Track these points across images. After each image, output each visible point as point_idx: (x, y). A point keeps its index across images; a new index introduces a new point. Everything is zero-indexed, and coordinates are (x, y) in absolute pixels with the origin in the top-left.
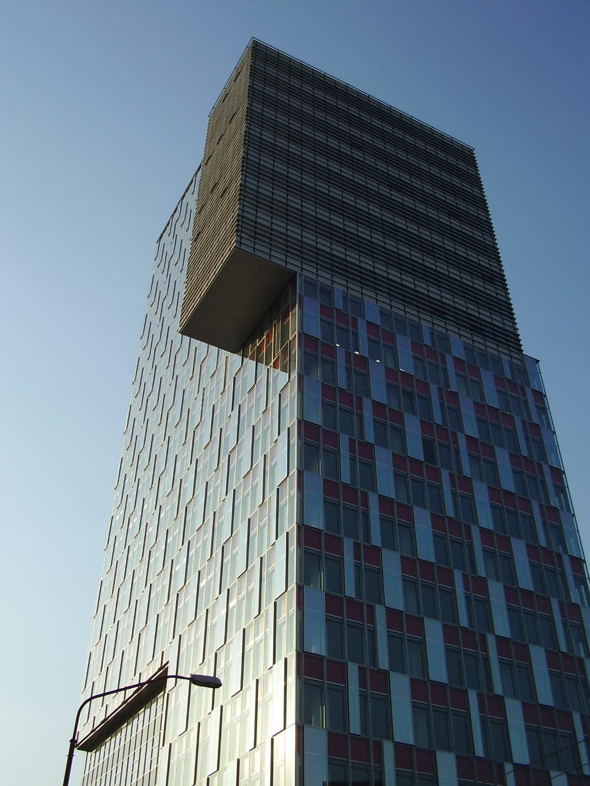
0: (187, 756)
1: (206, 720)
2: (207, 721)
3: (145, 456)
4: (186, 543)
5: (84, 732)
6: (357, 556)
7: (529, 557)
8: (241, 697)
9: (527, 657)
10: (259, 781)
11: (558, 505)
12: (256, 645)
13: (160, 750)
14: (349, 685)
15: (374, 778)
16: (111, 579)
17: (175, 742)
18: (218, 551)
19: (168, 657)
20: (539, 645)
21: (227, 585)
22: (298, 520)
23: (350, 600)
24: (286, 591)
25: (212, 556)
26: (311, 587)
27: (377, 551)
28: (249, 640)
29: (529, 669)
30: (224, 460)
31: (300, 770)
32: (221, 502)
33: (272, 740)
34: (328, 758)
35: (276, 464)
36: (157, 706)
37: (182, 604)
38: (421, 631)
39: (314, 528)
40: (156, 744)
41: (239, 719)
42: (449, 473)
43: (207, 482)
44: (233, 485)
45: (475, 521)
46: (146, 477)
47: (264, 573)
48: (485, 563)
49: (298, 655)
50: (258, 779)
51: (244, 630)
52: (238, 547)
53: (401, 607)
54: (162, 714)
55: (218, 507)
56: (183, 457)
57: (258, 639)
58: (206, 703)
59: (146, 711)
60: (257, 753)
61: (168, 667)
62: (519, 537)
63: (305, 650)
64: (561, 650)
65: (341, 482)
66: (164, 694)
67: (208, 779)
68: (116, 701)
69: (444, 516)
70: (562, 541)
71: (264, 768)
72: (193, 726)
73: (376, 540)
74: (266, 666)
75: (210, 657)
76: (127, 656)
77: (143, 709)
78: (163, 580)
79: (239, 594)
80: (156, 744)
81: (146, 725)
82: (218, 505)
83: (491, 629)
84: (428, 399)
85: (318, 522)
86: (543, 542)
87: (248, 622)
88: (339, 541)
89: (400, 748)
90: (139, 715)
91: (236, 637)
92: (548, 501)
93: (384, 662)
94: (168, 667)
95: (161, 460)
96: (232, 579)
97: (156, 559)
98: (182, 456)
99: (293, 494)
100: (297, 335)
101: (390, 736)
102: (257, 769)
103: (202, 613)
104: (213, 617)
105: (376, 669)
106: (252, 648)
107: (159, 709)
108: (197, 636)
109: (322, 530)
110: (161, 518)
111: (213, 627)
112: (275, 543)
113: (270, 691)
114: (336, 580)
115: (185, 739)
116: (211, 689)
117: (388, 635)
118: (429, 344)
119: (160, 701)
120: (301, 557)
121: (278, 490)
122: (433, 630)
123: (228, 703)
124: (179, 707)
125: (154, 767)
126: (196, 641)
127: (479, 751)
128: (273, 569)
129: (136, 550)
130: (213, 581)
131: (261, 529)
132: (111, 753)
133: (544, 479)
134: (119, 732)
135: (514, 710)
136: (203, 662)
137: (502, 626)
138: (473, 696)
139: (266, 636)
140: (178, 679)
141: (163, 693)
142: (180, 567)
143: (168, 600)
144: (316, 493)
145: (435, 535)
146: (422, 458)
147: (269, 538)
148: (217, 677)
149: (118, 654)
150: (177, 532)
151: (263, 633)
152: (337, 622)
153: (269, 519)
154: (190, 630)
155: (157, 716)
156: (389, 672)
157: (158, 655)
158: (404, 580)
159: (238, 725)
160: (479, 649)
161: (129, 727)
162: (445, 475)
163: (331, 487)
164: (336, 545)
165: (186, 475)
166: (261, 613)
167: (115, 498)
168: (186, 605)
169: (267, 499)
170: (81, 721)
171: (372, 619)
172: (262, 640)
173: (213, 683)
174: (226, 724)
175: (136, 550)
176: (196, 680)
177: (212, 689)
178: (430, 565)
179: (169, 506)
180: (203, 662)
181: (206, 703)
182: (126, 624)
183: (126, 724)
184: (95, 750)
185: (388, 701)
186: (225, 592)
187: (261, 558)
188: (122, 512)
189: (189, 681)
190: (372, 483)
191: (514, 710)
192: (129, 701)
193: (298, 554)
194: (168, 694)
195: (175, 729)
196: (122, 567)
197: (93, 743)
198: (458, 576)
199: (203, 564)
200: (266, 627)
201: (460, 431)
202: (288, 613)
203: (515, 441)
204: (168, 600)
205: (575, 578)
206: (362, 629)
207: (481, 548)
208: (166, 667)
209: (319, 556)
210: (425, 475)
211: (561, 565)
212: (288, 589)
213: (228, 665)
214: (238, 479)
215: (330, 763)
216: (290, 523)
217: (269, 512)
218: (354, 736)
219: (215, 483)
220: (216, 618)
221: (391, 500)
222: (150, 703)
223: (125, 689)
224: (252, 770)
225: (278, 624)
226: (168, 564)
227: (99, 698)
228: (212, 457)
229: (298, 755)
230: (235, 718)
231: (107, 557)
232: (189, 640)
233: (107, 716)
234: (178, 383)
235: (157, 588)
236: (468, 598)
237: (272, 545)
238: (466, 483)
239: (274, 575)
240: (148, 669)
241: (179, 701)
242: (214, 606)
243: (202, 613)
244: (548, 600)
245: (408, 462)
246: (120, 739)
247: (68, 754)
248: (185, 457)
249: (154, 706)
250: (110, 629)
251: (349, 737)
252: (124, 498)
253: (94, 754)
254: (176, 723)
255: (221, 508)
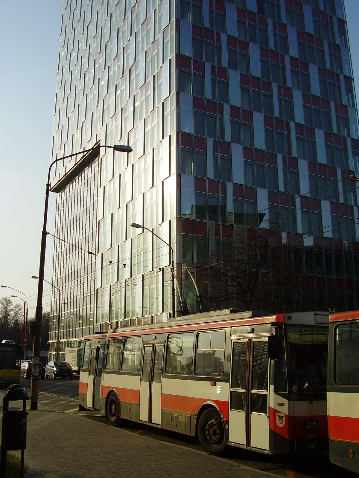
0: (114, 192)
1: (124, 172)
2: (125, 172)
3: (77, 12)
4: (107, 68)
5: (54, 182)
6: (213, 73)
7: (320, 75)
8: (144, 159)
9: (313, 136)
10: (156, 205)
11: (340, 43)
12: (152, 128)
13: (99, 190)
14: (207, 150)
15: (221, 203)
16: (59, 137)
17: (107, 185)
18: (127, 72)
19: (100, 136)
20: (314, 64)
21: (133, 93)
22: (177, 50)
23: (206, 29)
24: (169, 96)
25: (124, 75)
26: (185, 93)
27: (225, 70)
28: (147, 123)
29: (314, 142)
30: (129, 14)
31: (179, 208)
32: (128, 41)
33: (163, 182)
34: (195, 192)
35: (162, 15)
36: (95, 165)
37: (107, 105)
38: (251, 119)
39: (186, 56)
40: (96, 187)
41: (143, 171)
42: (273, 21)
43: (118, 28)
44: (135, 30)
45: (287, 52)
46: (79, 27)
47: (156, 85)
48: (292, 77)
49: (177, 133)
50: (155, 204)
51: (145, 119)
52: (139, 69)
53: (239, 105)
54: (98, 170)
55: (126, 44)
56: (102, 12)
57: (153, 124)
58: (124, 163)
59: (89, 168)
60: (154, 189)
61: (100, 143)
62: (314, 63)
63: (181, 131)
64: (334, 132)
65: (203, 27)
66: (99, 158)
67: (127, 205)
68: (71, 163)
69: (273, 116)
70: (340, 66)
71: (158, 198)
72: (117, 176)
73: (225, 63)
74: (158, 141)
75: (125, 136)
76: (75, 138)
77: (87, 167)
78: (94, 91)
79: (141, 98)
80: (96, 187)
81: (89, 176)
82: (126, 43)
83: (293, 119)
84: (266, 31)
85: (189, 52)
86: (328, 66)
87: (147, 114)
88: (202, 64)
89: (236, 187)
90: (85, 171)
91: (140, 124)
92: (334, 40)
93: (228, 138)
94: (100, 143)
95: (88, 14)
96: (136, 89)
97: (89, 79)
98: (101, 12)
99: (173, 34)
100: (175, 20)
101: (230, 179)
102: (154, 199)
103: (119, 111)
104: (126, 113)
105: (223, 141)
106: (149, 130)
107: (97, 167)
108: (116, 124)
109: (193, 134)
110: (90, 52)
111: (126, 118)
112: (162, 66)
113: (161, 154)
114: (202, 167)
115: (112, 183)
116: (126, 153)
117: (231, 122)
118: (273, 48)
119: (97, 163)
120: (178, 74)
121: (163, 32)
122: (258, 119)
123: (137, 162)
124: (106, 232)
125: (95, 199)
126: (116, 127)
127: (282, 188)
128: (161, 82)
129: (76, 73)
130: (124, 91)
131: (153, 57)
132: (71, 193)
133: (333, 26)
134: (74, 181)
135: (303, 166)
136: (121, 139)
137: (299, 117)
138: (279, 158)
139: (158, 123)
140: (107, 148)
141: (98, 158)
142: (104, 83)
143: (98, 103)
144: (188, 34)
145: (262, 61)
146: (255, 11)
147: (158, 63)
148: (130, 146)
149: (70, 136)
150: (101, 61)
151: (156, 121)
152: (201, 114)
153: (158, 51)
154: (112, 121)
155: (96, 171)
156: (231, 143)
157: (94, 136)
158: (242, 88)
159: (143, 175)
160: (285, 130)
161: (80, 178)
162: (270, 22)
163: (197, 30)
164: (200, 67)
165: (105, 24)
166: (155, 109)
167: (60, 41)
168: (109, 106)
169: (156, 38)
170: (52, 171)
171: (222, 112)
172: (156, 125)
173: (127, 149)
174: (136, 174)
175: (76, 73)
176: (117, 148)
177: (127, 153)
178: (258, 79)
179: (95, 45)
180: (121, 139)
181: (124, 163)
182: (74, 119)
183: (78, 176)
184: (61, 192)
185: (230, 160)
186: (132, 97)
187: (154, 76)
188: (66, 50)
189: (113, 149)
190: (223, 27)
191: (303, 166)
192: (78, 163)
193: (178, 239)
194: (101, 159)
195: (106, 178)
196: (68, 85)
197: (60, 188)
198: (275, 86)
199: (118, 80)
200: (158, 117)
201: (286, 54)
202: (171, 109)
203: (323, 57)
204: (98, 103)
205: (339, 31)
206: (215, 118)
207: (290, 69)
208: (99, 143)
209: (190, 74)
210: (257, 22)
211: (338, 81)
212: (171, 94)
213: (135, 141)
214: (138, 25)
215: (196, 195)
216: (171, 54)
217: (158, 46)
218: (210, 180)
219: (123, 29)
220: (128, 113)
221: (235, 38)
222: (91, 164)
223: (76, 154)
224: (151, 199)
225: (165, 115)
226: (97, 81)
227: (61, 160)
228: (120, 12)
229: (177, 148)
230: (141, 170)
231: (59, 78)
232: (112, 127)
233: (67, 172)
234: (93, 5)
235: (91, 96)
236: (280, 100)
237: (160, 68)
238: (283, 27)
239: (162, 18)
240: (89, 144)
241: (108, 162)
242: (126, 105)
243: (119, 111)
244: (329, 102)
245: (250, 79)
246: (75, 185)
247: (46, 193)
248: (103, 12)
249: (93, 165)
250: (64, 122)
251: (205, 100)
252: (66, 39)
253: (61, 194)
254: (107, 174)
255: (128, 44)
